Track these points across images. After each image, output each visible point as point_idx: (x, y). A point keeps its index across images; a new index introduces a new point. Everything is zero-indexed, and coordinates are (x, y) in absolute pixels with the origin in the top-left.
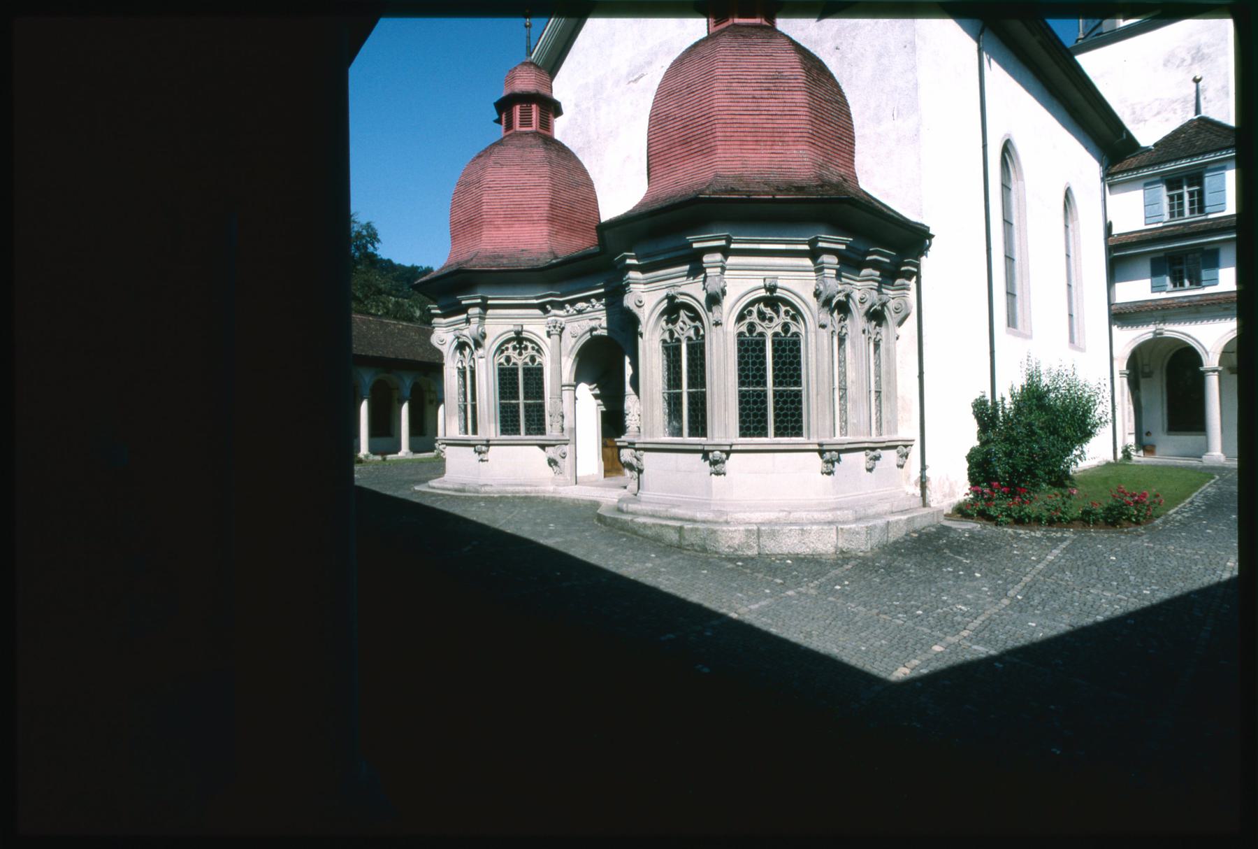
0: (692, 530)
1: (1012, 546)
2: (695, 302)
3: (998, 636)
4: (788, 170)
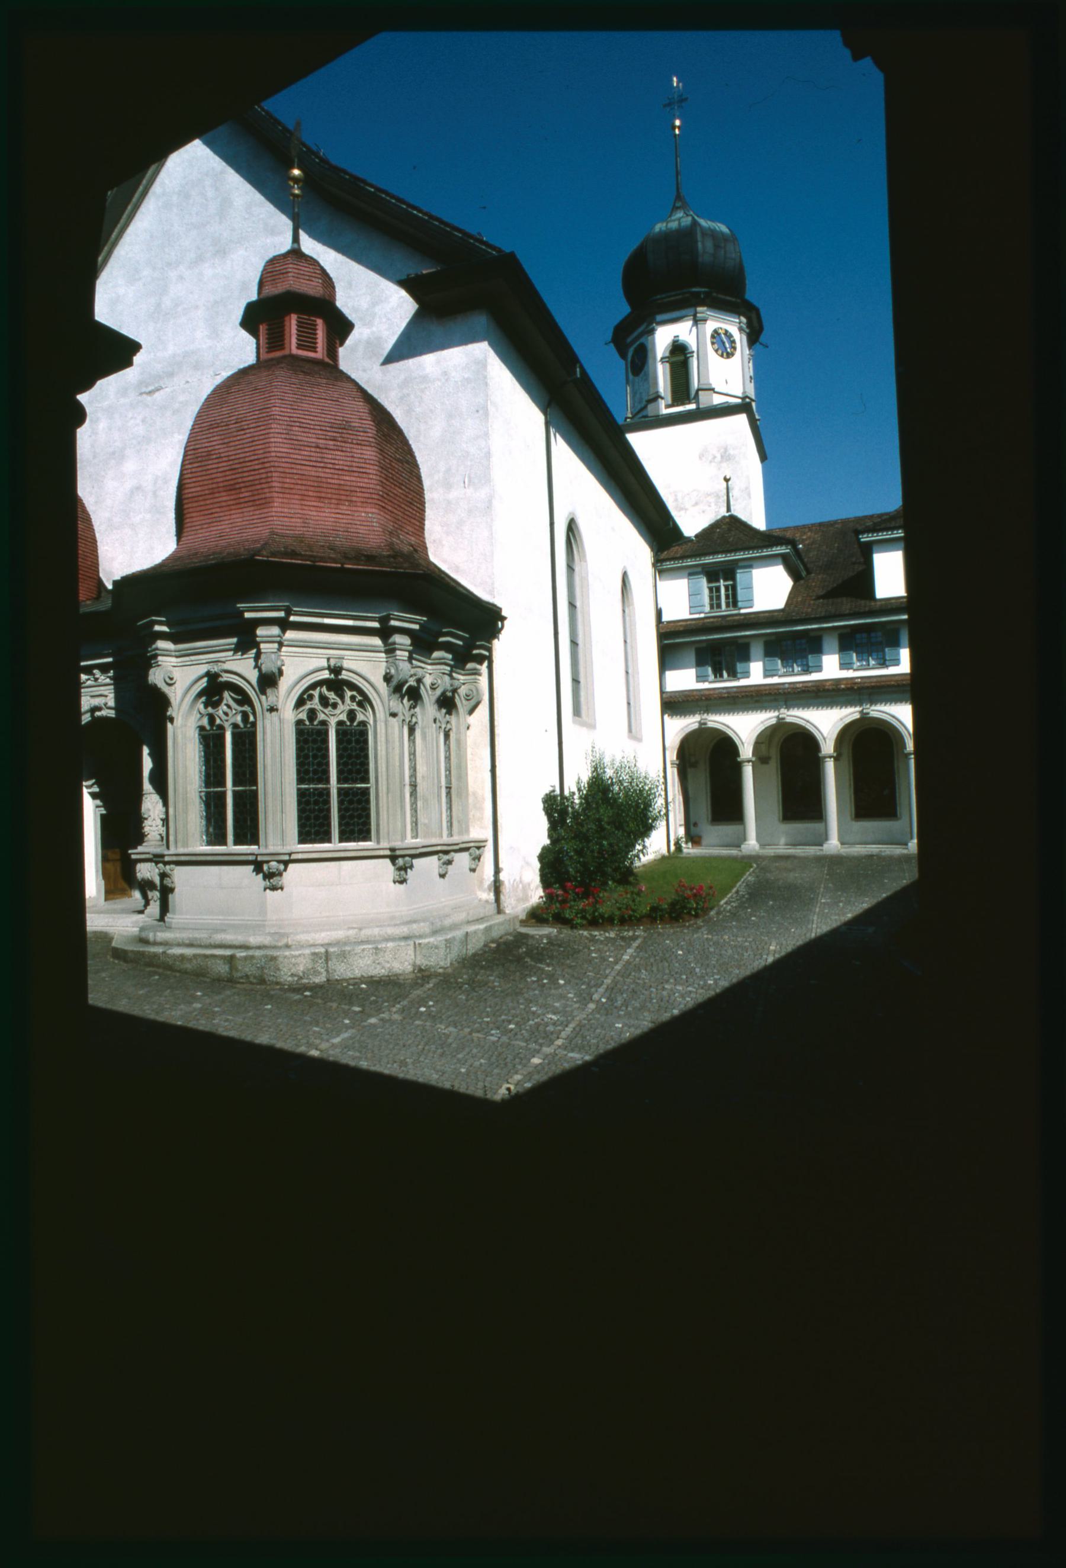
0: (246, 958)
1: (589, 949)
2: (237, 677)
3: (590, 1041)
4: (356, 535)
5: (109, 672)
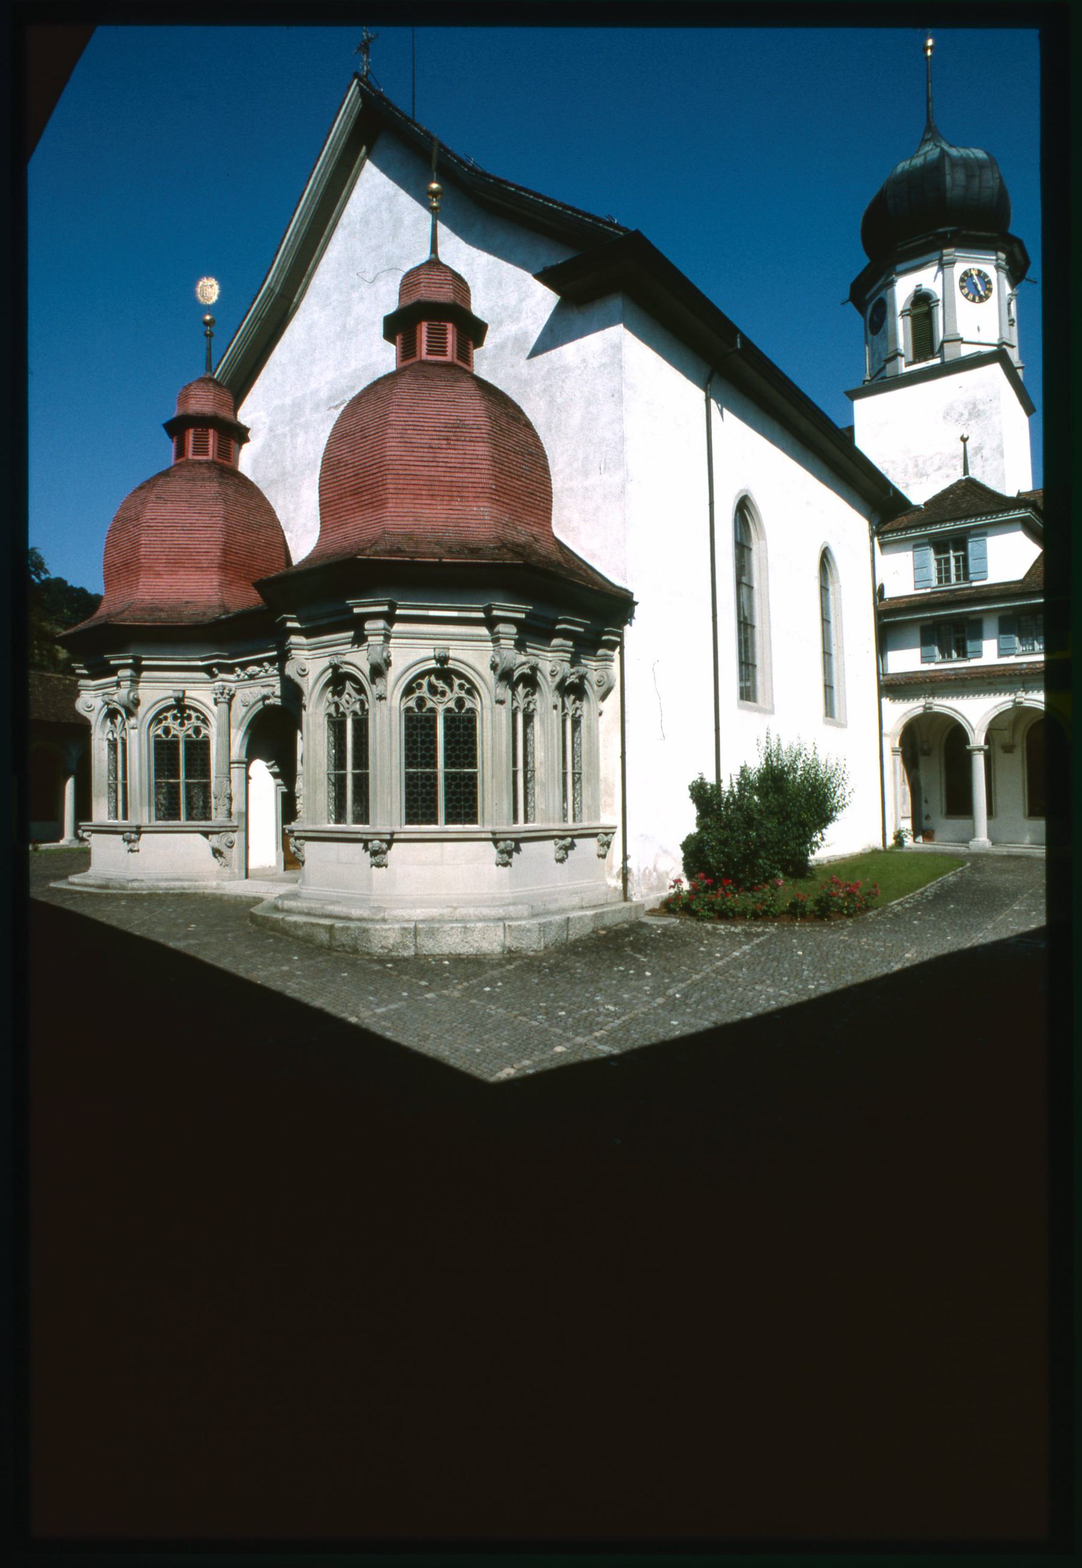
0: (342, 929)
4: (467, 529)
5: (275, 665)
